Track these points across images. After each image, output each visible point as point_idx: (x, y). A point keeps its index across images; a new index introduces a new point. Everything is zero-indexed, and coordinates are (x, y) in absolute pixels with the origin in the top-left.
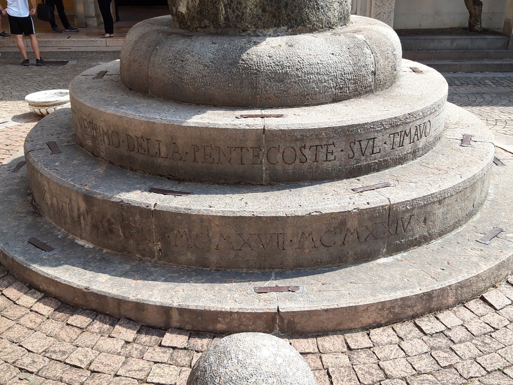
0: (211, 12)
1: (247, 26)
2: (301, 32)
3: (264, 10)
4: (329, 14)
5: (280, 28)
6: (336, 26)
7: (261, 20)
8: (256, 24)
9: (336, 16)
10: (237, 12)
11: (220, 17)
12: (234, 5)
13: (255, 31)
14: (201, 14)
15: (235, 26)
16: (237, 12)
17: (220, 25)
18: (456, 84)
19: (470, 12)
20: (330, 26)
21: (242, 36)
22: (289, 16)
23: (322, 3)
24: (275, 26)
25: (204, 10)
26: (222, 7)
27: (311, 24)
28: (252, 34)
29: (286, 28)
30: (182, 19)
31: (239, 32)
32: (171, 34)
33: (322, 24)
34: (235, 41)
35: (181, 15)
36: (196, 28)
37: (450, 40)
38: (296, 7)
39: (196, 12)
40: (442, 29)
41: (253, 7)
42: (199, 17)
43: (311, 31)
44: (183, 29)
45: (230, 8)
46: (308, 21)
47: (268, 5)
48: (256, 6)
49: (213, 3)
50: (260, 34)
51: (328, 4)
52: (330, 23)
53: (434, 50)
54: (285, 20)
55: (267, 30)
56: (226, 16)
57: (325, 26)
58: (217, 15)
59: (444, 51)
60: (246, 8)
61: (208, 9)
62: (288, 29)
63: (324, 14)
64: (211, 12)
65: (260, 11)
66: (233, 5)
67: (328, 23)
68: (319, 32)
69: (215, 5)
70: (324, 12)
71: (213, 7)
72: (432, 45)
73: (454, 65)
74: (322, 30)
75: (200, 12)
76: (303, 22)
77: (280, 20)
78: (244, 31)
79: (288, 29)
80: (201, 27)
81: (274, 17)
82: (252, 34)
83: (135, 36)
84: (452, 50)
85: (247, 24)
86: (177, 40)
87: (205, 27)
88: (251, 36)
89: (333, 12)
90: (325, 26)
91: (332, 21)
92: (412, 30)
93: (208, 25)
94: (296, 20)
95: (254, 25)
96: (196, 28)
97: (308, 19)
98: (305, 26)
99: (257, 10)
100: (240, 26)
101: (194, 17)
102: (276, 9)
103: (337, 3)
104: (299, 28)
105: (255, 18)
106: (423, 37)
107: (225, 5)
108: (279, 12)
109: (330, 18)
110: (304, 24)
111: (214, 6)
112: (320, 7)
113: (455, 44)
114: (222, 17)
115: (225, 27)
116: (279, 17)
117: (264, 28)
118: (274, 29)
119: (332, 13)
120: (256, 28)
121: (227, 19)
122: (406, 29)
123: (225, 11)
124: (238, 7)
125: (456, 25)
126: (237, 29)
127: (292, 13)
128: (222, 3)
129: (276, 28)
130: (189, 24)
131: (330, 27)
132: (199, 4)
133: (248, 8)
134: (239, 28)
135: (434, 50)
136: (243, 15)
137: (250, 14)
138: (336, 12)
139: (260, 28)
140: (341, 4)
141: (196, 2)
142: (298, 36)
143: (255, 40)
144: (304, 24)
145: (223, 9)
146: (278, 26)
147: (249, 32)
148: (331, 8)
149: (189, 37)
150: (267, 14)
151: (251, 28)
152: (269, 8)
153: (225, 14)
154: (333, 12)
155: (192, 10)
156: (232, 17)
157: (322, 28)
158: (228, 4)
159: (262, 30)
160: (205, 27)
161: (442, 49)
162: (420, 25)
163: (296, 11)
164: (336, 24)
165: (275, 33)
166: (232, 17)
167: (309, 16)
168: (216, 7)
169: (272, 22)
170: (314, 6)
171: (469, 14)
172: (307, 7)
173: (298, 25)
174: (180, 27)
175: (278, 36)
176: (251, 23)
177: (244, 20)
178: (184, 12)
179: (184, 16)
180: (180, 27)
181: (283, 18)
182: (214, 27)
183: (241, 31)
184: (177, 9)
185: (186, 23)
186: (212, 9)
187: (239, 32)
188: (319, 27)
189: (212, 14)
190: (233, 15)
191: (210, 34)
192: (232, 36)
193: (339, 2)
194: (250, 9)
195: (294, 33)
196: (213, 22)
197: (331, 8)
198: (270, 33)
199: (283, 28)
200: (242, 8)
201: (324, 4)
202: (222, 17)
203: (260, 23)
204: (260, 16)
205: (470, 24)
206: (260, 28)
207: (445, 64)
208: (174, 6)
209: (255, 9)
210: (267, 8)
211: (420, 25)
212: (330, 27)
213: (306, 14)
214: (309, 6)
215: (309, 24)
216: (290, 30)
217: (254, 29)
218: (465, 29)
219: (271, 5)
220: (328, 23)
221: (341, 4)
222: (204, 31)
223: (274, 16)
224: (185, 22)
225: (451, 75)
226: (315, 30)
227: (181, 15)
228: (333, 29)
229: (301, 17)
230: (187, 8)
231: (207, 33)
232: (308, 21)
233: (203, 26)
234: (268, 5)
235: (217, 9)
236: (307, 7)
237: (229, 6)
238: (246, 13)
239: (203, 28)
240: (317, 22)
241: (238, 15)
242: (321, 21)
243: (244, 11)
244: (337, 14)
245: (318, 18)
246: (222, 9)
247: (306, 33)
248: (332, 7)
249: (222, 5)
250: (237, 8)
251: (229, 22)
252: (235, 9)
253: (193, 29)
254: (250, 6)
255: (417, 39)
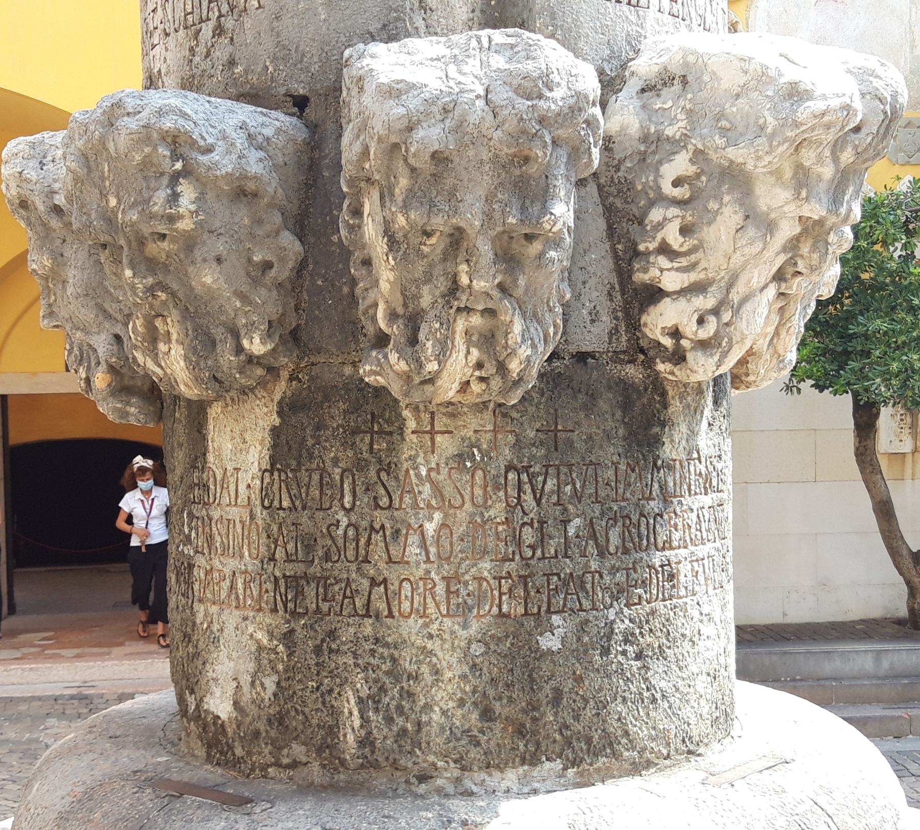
0: (314, 722)
1: (434, 764)
2: (605, 776)
3: (487, 714)
4: (686, 712)
5: (538, 768)
6: (707, 745)
7: (478, 744)
8: (462, 758)
9: (705, 716)
10: (400, 721)
11: (345, 735)
12: (392, 699)
13: (458, 780)
14: (280, 724)
15: (395, 765)
16: (400, 721)
17: (343, 762)
18: (913, 772)
19: (908, 583)
20: (692, 747)
21: (416, 796)
22: (567, 727)
23: (663, 684)
24: (523, 762)
25: (293, 713)
26: (349, 704)
27: (634, 748)
28: (450, 789)
29: (558, 765)
30: (215, 733)
31: (407, 782)
32: (182, 790)
33: (668, 744)
34: (396, 820)
35: (215, 724)
36: (264, 768)
37: (870, 656)
38: (586, 701)
39: (264, 719)
40: (843, 624)
41: (451, 704)
42: (273, 733)
43: (637, 768)
44: (218, 764)
45: (377, 710)
46: (624, 741)
47: (500, 699)
48: (461, 703)
49: (322, 695)
50: (475, 789)
51: (680, 683)
52: (690, 738)
53: (835, 679)
54: (555, 741)
55: (497, 774)
56: (363, 732)
57: (677, 750)
58: (332, 730)
59: (859, 682)
60: (427, 707)
61: (304, 714)
62: (565, 768)
63: (673, 712)
64: (314, 722)
65: (475, 716)
66: (387, 699)
67: (684, 741)
68: (660, 770)
69: (328, 699)
70: (670, 707)
71: (320, 706)
72: (829, 667)
73: (893, 718)
74: (667, 762)
75: (280, 720)
76: (611, 744)
77: (538, 744)
78: (423, 778)
79: (565, 768)
80: (278, 764)
81: (521, 733)
82: (450, 789)
83: (60, 793)
84: (879, 678)
85: (431, 758)
86: (203, 820)
87: (294, 765)
88: (447, 796)
89: (695, 705)
90: (677, 750)
91: (695, 733)
92: (767, 627)
93: (304, 759)
94: (589, 741)
95: (455, 762)
96: (264, 768)
97: (626, 733)
98: (615, 755)
99: (463, 716)
100: (410, 765)
101: (257, 734)
102: (524, 711)
103: (705, 675)
104: (599, 764)
105: (458, 740)
106: (802, 648)
107: (360, 701)
108: (535, 720)
109: (689, 724)
110: (612, 749)
111: (324, 703)
112: (658, 696)
113: (885, 664)
114: (351, 738)
115: (362, 766)
116: (534, 733)
117: (487, 767)
118: (521, 770)
119: (693, 707)
120: (463, 769)
121: (366, 742)
122: (752, 626)
123: (362, 717)
124: (403, 707)
125: (876, 613)
126: (399, 773)
127: (577, 718)
128: (350, 693)
129: (526, 767)
130: (239, 752)
131: (690, 752)
132: (275, 695)
133: (436, 709)
134: (406, 769)
135: (835, 679)
136: (419, 730)
137: (442, 729)
138: (703, 702)
139: (476, 768)
140: (715, 678)
141: (264, 689)
142: (599, 789)
143: (464, 816)
144: (612, 749)
145: (356, 713)
146: (532, 760)
147: (440, 782)
148: (688, 693)
149: (240, 802)
150: (498, 726)
151: (446, 770)
152: (502, 706)
153: (362, 726)
154: (695, 705)
155: (253, 710)
156: (385, 737)
157: (668, 757)
158: (369, 697)
159: (483, 775)
160: (294, 765)
161: (855, 678)
162: (785, 615)
163: (589, 713)
164: (705, 741)
165: (524, 781)
166: (385, 737)
167: (626, 724)
168: (332, 706)
169: (513, 749)
170: (640, 694)
171: (905, 588)
172: (619, 700)
173: (596, 755)
174: (209, 759)
175: (535, 792)
176: (445, 756)
177: (424, 745)
178: (224, 716)
179: (222, 725)
180: (209, 759)
181: (548, 737)
182: (323, 766)
183: (413, 780)
184: (201, 701)
185: (231, 748)
186: (317, 710)
187: (407, 782)
188: (659, 755)
189: (318, 725)
190: (386, 730)
191: (308, 789)
192: (383, 795)
193: (709, 674)
194: (444, 713)
195: (584, 782)
196: (320, 751)
197: (688, 693)
198: (509, 784)
199: (548, 765)
200: (417, 709)
201: (670, 685)
202: (351, 738)
203: (474, 753)
204: (475, 733)
205: (911, 610)
206: (476, 768)
207: (869, 717)
208: (192, 692)
209: (459, 712)
210: (497, 707)
211: (785, 615)
212: (690, 752)
213: (619, 719)
214: (627, 694)
215: (628, 750)
216: (571, 772)
217: (457, 773)
218: (900, 622)
219: (511, 697)
220: (684, 741)
221: (715, 678)
222: (291, 779)
223: (520, 732)
224: (227, 743)
225: (893, 745)
226: (649, 764)
227: (215, 724)
228: (699, 755)
229: (603, 731)
230: (236, 704)
231: (299, 785)
232: (624, 741)
233: (285, 761)
234: (500, 699)
235: (335, 713)
236: (619, 700)
237: (374, 702)
238: (429, 723)
239: (288, 767)
240: (654, 740)
241: (404, 731)
242: (662, 737)
243: (424, 718)
244: (707, 707)
245: (654, 728)
246: (351, 713)
247: (621, 776)
248: (692, 690)
249: (352, 701)
250: (400, 709)
251: (373, 752)
252: (393, 710)
253: (253, 770)
254: (442, 704)
255: (785, 653)
